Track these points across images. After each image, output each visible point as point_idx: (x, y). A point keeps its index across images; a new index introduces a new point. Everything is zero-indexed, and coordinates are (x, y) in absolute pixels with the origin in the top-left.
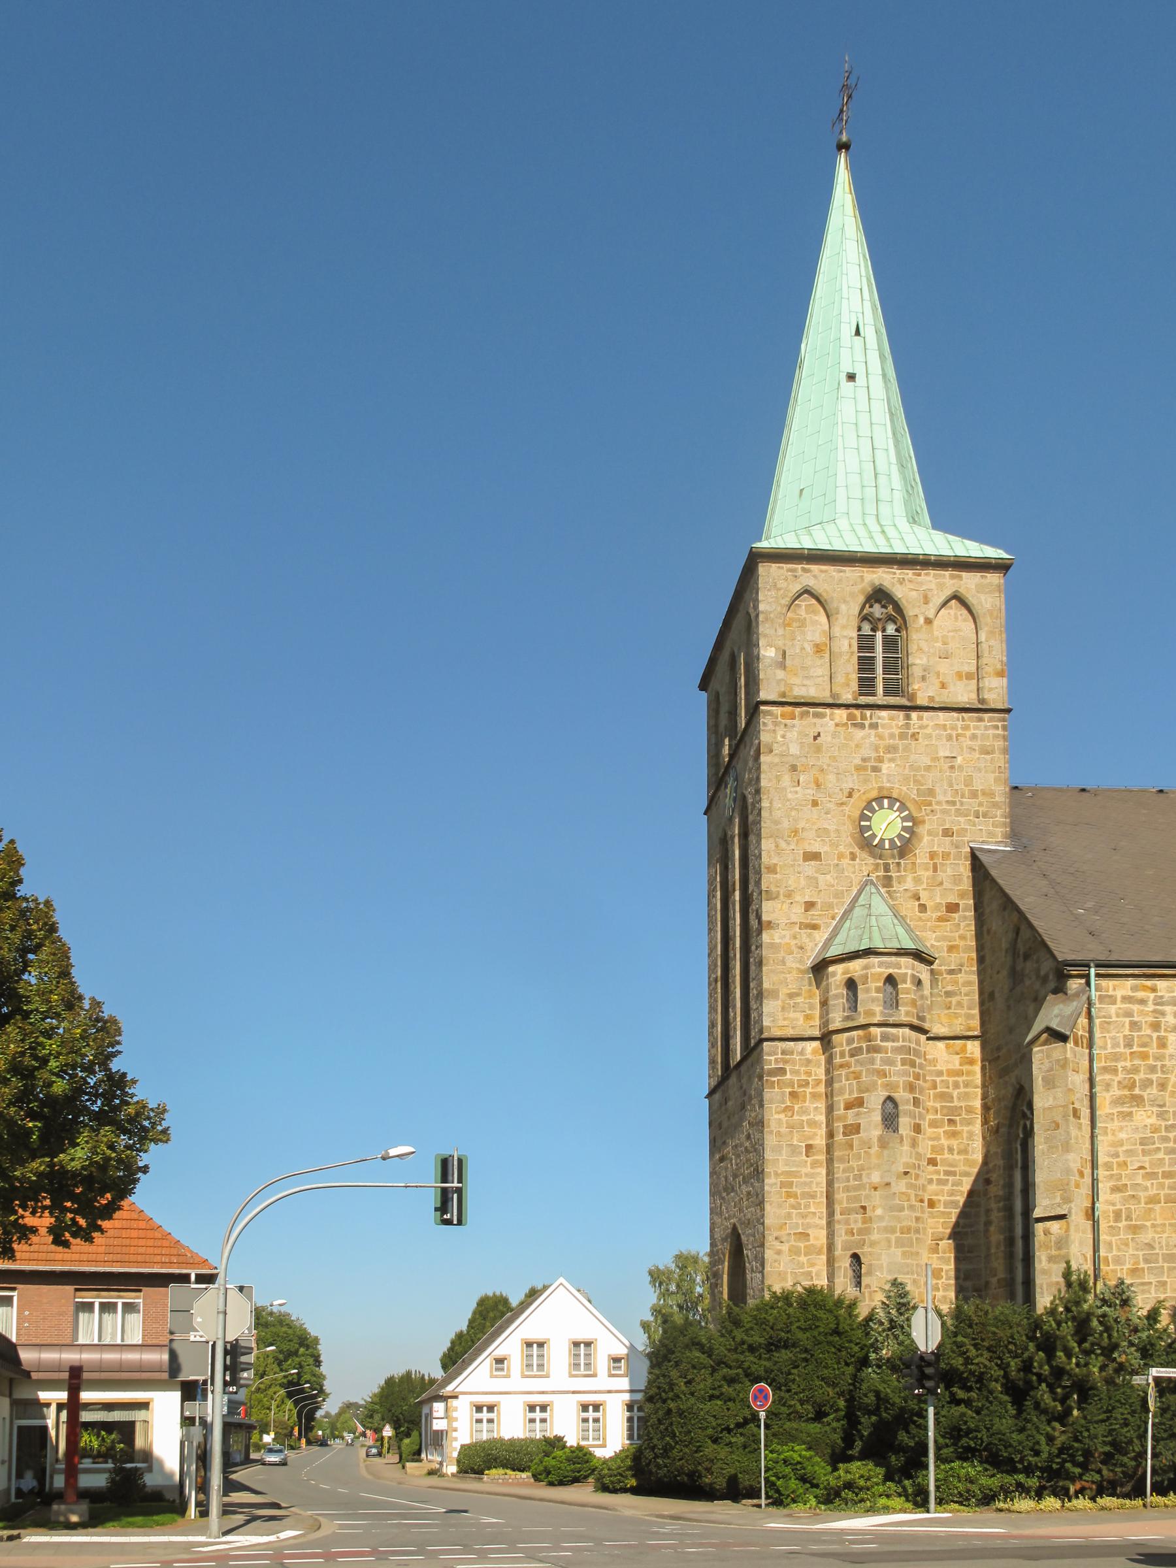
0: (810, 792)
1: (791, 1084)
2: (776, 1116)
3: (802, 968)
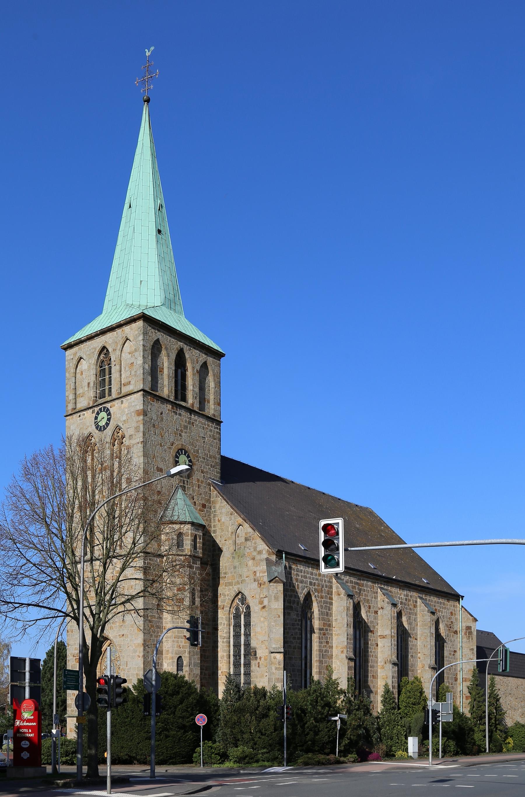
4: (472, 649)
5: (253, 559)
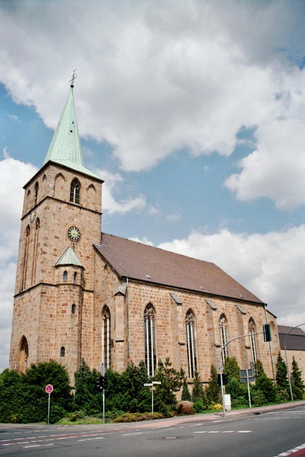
0: (57, 222)
1: (48, 297)
2: (43, 305)
3: (53, 266)
4: (276, 335)
5: (112, 284)
